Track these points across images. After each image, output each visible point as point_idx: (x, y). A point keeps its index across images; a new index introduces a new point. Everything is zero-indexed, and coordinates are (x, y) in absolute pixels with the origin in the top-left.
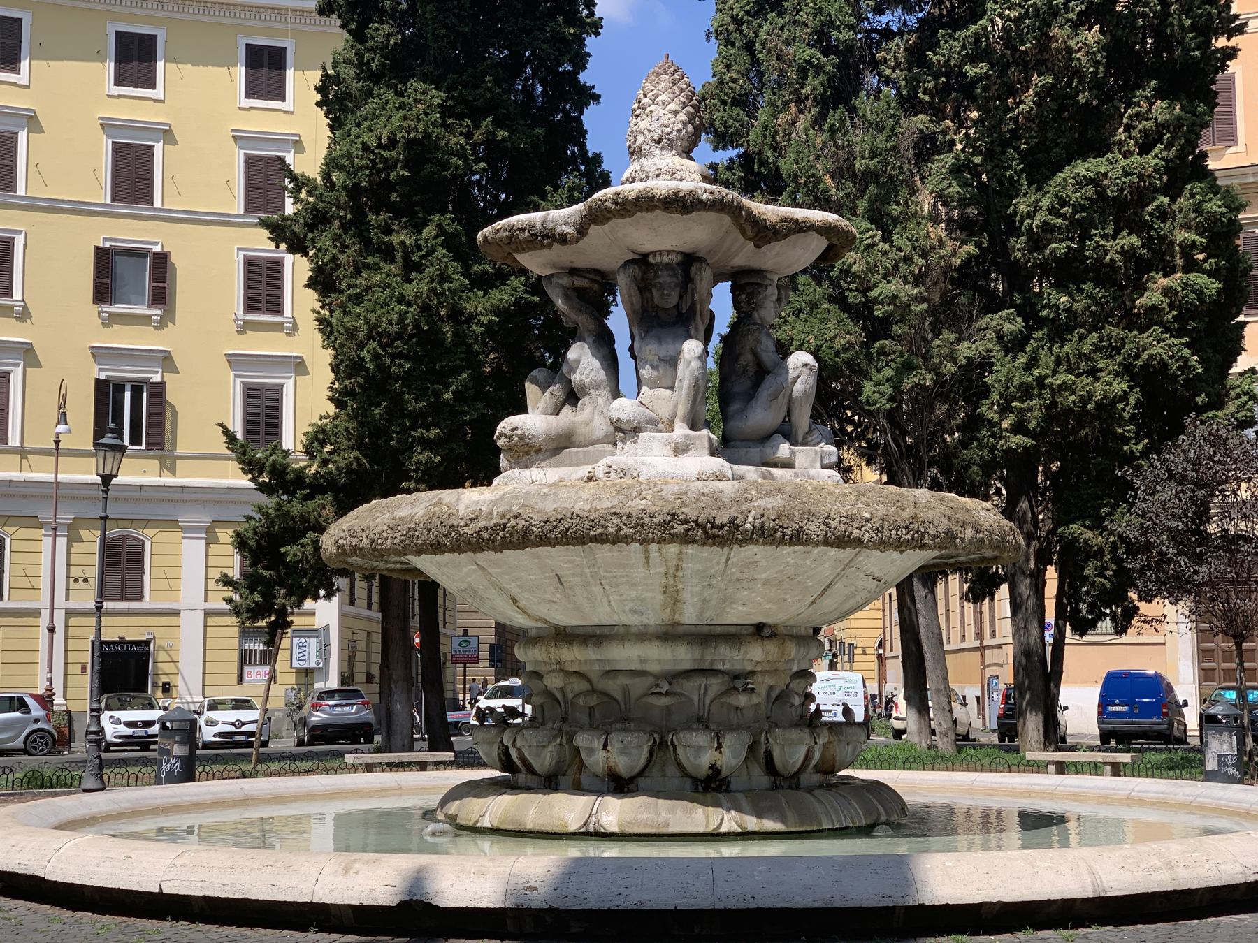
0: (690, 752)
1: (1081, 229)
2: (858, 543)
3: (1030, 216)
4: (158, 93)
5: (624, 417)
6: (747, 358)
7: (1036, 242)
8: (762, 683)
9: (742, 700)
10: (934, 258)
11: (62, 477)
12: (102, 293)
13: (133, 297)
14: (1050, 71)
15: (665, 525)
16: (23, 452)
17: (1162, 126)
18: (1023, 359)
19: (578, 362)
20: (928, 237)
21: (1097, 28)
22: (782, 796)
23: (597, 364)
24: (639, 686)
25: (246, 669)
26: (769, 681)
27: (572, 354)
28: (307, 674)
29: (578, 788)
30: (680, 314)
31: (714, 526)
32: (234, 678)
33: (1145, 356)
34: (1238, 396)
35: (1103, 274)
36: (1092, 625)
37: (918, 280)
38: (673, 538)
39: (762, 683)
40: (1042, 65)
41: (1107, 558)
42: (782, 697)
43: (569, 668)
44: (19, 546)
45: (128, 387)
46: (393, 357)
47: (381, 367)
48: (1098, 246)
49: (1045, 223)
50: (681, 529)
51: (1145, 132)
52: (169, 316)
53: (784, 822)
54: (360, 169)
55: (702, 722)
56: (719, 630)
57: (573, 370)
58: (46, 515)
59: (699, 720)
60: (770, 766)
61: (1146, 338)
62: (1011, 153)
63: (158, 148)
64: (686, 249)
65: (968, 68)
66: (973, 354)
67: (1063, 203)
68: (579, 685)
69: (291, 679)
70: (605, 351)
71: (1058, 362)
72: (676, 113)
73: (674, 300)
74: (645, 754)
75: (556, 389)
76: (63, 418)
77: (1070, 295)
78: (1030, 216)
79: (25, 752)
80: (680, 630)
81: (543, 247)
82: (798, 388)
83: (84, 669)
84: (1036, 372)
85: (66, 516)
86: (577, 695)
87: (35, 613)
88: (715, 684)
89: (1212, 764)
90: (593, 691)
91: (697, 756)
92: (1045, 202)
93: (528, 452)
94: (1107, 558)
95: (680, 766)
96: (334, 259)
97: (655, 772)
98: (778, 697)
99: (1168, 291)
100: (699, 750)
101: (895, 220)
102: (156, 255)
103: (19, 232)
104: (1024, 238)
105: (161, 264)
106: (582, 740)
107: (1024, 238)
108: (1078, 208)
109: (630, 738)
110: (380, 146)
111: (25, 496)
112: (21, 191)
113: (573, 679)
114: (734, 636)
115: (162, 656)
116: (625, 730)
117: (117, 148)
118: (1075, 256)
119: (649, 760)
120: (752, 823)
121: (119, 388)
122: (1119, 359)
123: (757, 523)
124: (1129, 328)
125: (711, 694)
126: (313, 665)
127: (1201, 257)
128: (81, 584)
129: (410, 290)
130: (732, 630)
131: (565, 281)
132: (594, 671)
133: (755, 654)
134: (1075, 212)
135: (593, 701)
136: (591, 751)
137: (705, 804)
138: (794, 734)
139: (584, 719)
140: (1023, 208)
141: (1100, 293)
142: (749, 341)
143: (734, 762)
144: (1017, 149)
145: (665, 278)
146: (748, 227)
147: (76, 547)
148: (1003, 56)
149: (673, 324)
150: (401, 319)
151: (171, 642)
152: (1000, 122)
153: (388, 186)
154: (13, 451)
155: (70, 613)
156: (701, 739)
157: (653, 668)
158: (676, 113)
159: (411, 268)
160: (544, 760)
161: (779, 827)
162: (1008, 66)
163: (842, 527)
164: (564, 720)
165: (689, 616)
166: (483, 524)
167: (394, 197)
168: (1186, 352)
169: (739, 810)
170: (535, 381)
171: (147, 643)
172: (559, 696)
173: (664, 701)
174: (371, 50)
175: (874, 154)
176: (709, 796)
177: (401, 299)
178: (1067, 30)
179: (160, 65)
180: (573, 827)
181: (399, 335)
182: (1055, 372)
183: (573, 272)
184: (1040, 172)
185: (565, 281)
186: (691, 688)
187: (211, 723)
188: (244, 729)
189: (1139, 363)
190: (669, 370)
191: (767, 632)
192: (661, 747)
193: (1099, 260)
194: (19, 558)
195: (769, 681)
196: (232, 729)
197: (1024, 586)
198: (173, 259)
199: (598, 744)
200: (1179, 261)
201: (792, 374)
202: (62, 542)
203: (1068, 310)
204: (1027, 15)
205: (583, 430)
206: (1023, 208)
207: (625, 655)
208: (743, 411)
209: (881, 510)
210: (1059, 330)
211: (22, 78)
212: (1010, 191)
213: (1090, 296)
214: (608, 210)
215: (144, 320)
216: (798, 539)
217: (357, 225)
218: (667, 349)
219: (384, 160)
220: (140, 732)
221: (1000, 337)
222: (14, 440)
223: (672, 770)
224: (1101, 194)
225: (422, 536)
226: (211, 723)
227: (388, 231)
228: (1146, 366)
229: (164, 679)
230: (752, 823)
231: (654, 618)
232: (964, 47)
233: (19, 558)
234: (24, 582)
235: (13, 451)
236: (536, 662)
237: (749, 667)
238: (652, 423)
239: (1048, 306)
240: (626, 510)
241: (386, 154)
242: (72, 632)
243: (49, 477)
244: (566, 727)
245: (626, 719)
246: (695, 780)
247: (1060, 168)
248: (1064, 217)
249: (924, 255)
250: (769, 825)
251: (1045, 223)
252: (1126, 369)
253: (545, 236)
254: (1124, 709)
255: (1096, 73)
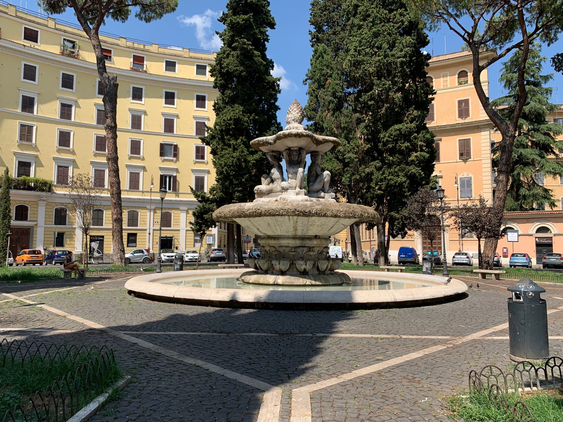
0: (299, 266)
1: (396, 141)
2: (340, 217)
3: (383, 138)
4: (175, 106)
5: (284, 186)
6: (314, 172)
7: (385, 144)
8: (316, 250)
9: (312, 253)
10: (360, 148)
11: (152, 198)
12: (162, 154)
13: (169, 155)
14: (389, 103)
15: (293, 212)
16: (143, 192)
17: (415, 117)
18: (381, 172)
19: (274, 173)
20: (359, 143)
21: (400, 93)
22: (321, 276)
23: (278, 173)
24: (287, 250)
25: (196, 244)
26: (318, 249)
27: (272, 171)
28: (210, 245)
29: (272, 274)
30: (298, 162)
31: (305, 212)
32: (193, 246)
33: (410, 172)
34: (433, 182)
35: (401, 152)
36: (396, 236)
37: (356, 153)
38: (296, 215)
39: (316, 250)
40: (387, 102)
41: (400, 220)
42: (321, 253)
43: (271, 245)
44: (142, 214)
45: (168, 177)
46: (231, 171)
47: (227, 173)
48: (400, 146)
49: (387, 140)
50: (298, 213)
51: (411, 118)
52: (178, 160)
53: (321, 282)
54: (223, 125)
55: (302, 258)
56: (306, 237)
57: (273, 175)
58: (148, 207)
59: (301, 258)
60: (318, 269)
61: (411, 168)
62: (379, 123)
63: (175, 119)
64: (300, 146)
65: (369, 102)
66: (369, 171)
67: (391, 135)
68: (273, 249)
69: (206, 246)
70: (280, 170)
71: (389, 173)
72: (298, 113)
73: (297, 159)
74: (288, 266)
75: (269, 179)
76: (152, 184)
77: (393, 157)
78: (383, 138)
79: (143, 263)
80: (297, 236)
81: (266, 145)
82: (326, 180)
83: (157, 243)
84: (384, 176)
85: (153, 207)
86: (273, 252)
87: (146, 230)
88: (305, 250)
89: (424, 270)
90: (277, 251)
91: (301, 267)
92: (387, 135)
93: (262, 194)
94: (400, 220)
95: (297, 269)
96: (217, 147)
97: (291, 270)
98: (320, 253)
99: (416, 157)
100: (301, 265)
101: (351, 139)
102: (175, 145)
103: (142, 139)
104: (382, 143)
105: (176, 147)
106: (274, 262)
107: (382, 143)
108: (395, 136)
109: (285, 262)
110: (228, 120)
111: (143, 202)
112: (142, 129)
113: (272, 248)
114: (310, 238)
115: (176, 240)
116: (284, 260)
117: (165, 119)
118: (394, 147)
119: (290, 267)
120: (314, 282)
121: (166, 177)
122: (404, 173)
123: (315, 212)
124: (407, 165)
125: (304, 252)
126: (211, 243)
127: (424, 148)
128: (157, 223)
129: (235, 155)
130: (309, 237)
131: (271, 154)
132: (277, 246)
133: (315, 242)
134: (394, 137)
135: (276, 253)
136: (276, 265)
137: (303, 278)
138: (324, 262)
139: (274, 257)
140: (382, 136)
141: (400, 157)
142: (315, 168)
143: (309, 268)
144: (381, 122)
145: (295, 153)
146: (315, 141)
147: (155, 214)
148: (378, 99)
149: (296, 164)
150: (232, 162)
151: (178, 237)
152: (377, 115)
153: (230, 130)
154: (141, 192)
155: (154, 230)
156: (301, 262)
157: (291, 245)
158: (298, 113)
159: (235, 149)
160: (265, 267)
161: (320, 283)
162: (379, 102)
163: (336, 213)
164: (270, 257)
165: (299, 233)
166: (251, 211)
167: (231, 132)
168: (420, 171)
169: (310, 279)
170: (264, 177)
171: (172, 237)
172: (268, 252)
173: (293, 253)
174: (226, 97)
175: (346, 123)
176: (304, 276)
177: (232, 157)
178: (393, 93)
179: (176, 100)
180: (271, 283)
181: (232, 165)
182: (389, 176)
183: (273, 151)
184: (386, 127)
185: (271, 154)
186: (299, 250)
187: (187, 256)
188: (195, 258)
189: (409, 174)
190: (295, 175)
191: (318, 237)
192: (292, 264)
193: (400, 149)
194: (142, 217)
195: (318, 249)
196: (192, 258)
197: (380, 227)
198: (179, 146)
199: (277, 263)
200: (419, 149)
201: (324, 176)
202: (152, 213)
203: (392, 161)
204: (383, 90)
205: (275, 189)
206: (382, 136)
207: (284, 242)
208: (313, 185)
209: (345, 209)
210: (390, 166)
211: (143, 102)
212: (379, 132)
213: (397, 157)
214: (281, 137)
215: (172, 161)
216: (325, 215)
217: (222, 139)
218: (295, 170)
219: (229, 123)
220: (170, 258)
221: (376, 167)
222: (141, 189)
223: (295, 270)
224: (401, 133)
225: (236, 214)
226: (187, 256)
227: (229, 140)
228: (410, 174)
229: (176, 246)
230: (314, 282)
231: (291, 233)
232: (368, 97)
233: (142, 217)
234: (143, 223)
235: (141, 192)
236: (263, 244)
237: (313, 246)
238: (291, 188)
239: (387, 160)
240: (284, 208)
241: (229, 122)
242: (154, 234)
243: (149, 198)
244: (270, 259)
245: (284, 257)
246: (300, 272)
247: (391, 127)
248: (391, 138)
249: (358, 147)
250: (318, 283)
251: (387, 140)
252: (406, 175)
253: (266, 143)
254: (404, 256)
255: (400, 104)
